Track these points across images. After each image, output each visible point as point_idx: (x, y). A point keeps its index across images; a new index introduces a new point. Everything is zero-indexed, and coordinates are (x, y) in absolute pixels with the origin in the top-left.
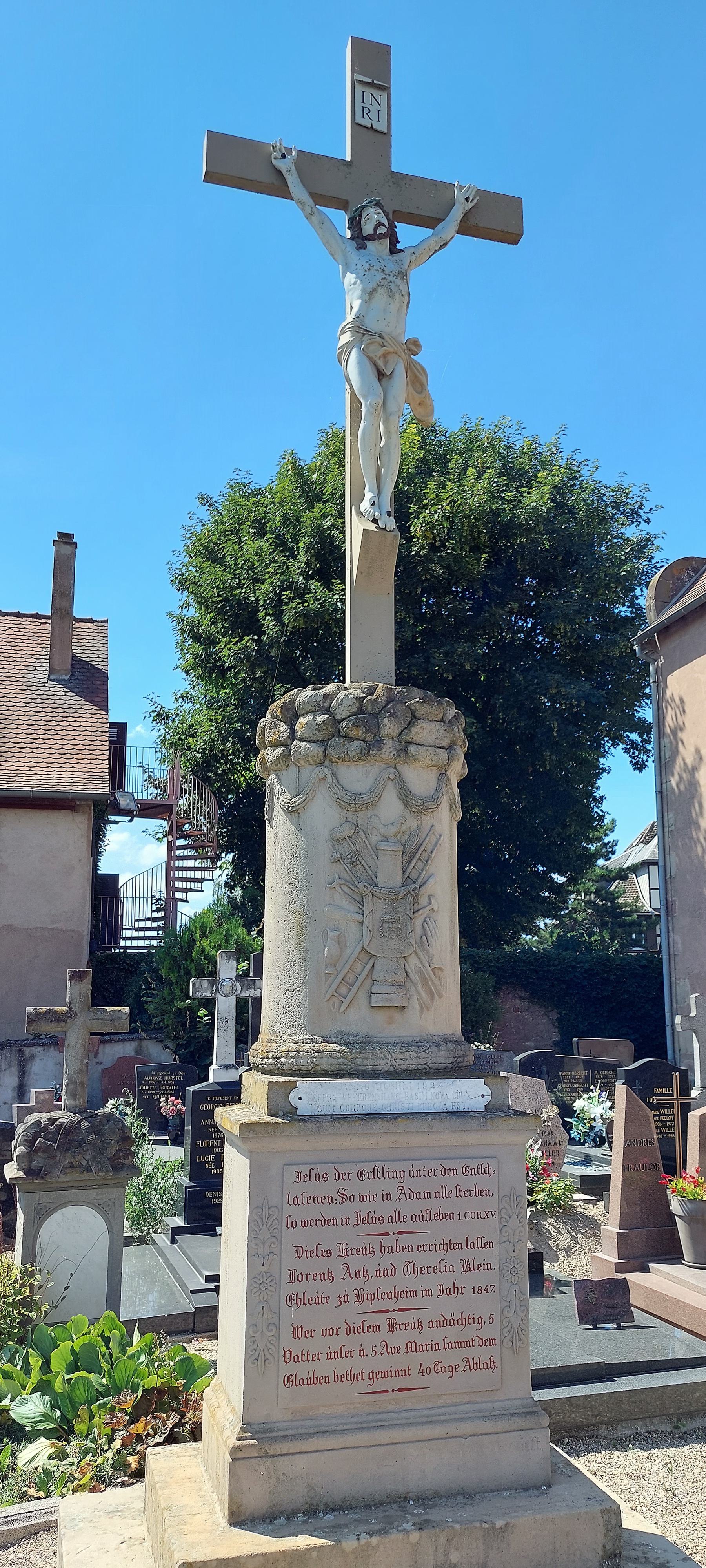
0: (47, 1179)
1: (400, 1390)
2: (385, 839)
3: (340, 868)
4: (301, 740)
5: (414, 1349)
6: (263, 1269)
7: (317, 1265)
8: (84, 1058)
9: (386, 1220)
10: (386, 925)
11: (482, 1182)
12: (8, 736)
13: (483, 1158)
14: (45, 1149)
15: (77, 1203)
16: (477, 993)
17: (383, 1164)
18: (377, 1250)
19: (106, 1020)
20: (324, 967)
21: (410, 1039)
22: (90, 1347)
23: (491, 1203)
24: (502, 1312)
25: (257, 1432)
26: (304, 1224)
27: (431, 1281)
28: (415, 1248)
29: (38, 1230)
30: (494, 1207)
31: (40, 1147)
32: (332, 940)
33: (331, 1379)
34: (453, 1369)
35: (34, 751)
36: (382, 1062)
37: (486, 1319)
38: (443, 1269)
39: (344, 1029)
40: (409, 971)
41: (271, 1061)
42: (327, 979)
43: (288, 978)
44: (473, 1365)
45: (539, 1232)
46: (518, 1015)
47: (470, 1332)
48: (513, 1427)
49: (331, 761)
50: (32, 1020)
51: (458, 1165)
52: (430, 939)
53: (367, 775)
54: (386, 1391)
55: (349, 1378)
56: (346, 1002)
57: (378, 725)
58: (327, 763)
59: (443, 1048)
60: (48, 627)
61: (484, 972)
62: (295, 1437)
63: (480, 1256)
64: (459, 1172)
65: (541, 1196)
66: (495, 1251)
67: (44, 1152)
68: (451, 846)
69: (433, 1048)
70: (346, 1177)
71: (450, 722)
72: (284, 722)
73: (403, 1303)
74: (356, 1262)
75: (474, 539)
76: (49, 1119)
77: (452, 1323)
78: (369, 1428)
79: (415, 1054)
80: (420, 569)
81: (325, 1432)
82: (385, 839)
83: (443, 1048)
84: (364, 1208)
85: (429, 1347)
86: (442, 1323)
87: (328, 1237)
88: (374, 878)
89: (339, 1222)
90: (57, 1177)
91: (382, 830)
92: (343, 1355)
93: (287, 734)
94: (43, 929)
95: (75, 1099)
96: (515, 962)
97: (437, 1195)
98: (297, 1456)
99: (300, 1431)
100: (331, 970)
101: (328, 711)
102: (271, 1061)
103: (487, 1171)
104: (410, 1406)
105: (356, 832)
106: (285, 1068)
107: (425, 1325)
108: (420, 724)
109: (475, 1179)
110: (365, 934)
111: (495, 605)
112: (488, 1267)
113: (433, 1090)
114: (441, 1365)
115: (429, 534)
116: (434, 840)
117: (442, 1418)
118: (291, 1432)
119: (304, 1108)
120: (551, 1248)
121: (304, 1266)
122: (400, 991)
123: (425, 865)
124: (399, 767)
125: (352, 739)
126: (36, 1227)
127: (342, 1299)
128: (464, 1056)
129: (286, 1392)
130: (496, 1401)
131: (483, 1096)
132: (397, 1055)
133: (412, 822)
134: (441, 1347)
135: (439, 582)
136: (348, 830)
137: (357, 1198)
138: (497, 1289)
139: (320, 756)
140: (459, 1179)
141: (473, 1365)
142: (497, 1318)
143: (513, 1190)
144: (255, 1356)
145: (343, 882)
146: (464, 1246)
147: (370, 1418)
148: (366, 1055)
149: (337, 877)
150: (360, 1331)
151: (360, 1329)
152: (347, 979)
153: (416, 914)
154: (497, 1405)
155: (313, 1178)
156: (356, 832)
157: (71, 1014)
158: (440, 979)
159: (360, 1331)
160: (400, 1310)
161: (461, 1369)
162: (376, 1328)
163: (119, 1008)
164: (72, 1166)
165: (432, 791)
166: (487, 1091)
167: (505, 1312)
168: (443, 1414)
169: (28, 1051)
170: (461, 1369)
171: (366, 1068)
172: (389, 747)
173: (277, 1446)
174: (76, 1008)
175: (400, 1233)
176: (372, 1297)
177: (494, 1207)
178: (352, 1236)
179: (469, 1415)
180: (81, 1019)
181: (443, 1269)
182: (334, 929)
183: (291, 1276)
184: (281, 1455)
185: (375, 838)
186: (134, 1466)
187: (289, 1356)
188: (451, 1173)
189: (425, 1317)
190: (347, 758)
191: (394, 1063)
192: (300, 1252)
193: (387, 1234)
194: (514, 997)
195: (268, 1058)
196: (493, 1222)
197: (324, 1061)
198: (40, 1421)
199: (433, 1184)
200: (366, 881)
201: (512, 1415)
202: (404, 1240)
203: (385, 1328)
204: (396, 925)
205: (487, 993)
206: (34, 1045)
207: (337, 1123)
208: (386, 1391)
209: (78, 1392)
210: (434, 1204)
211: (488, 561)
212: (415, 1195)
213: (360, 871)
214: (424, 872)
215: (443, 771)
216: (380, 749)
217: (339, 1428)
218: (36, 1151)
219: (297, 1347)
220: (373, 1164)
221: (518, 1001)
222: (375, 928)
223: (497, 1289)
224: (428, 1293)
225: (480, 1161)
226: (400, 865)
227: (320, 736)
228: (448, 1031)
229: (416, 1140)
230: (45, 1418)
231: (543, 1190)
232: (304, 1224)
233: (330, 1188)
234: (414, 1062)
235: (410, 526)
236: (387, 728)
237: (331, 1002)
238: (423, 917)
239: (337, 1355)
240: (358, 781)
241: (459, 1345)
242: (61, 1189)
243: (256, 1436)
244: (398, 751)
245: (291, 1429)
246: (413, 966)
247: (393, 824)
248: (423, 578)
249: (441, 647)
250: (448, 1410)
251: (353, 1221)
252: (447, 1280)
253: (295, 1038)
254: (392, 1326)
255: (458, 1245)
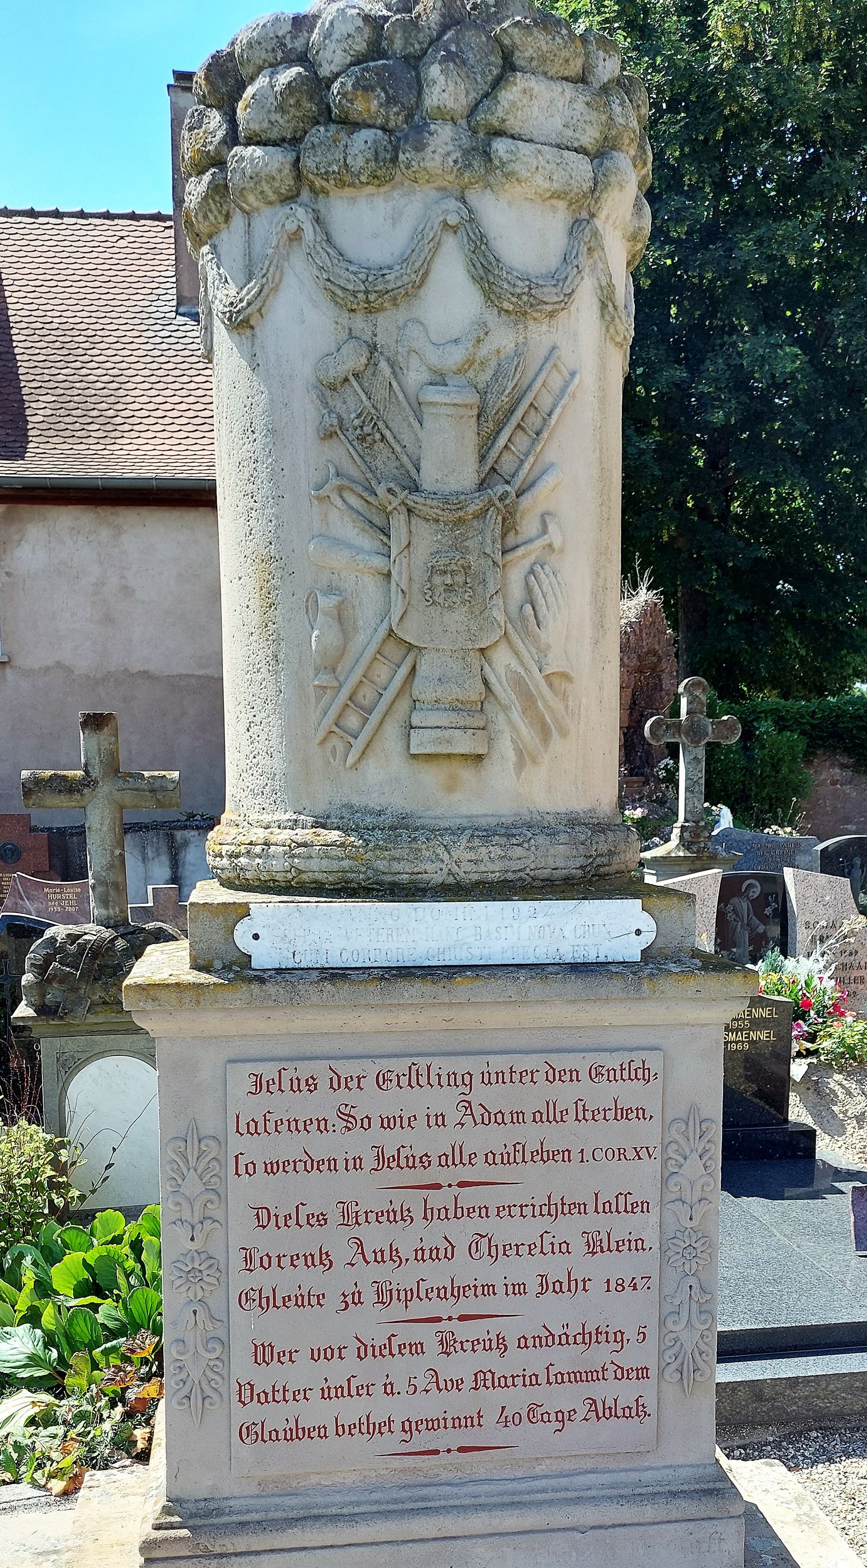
0: (68, 1020)
1: (461, 1450)
2: (439, 379)
3: (340, 453)
4: (250, 141)
5: (489, 1383)
6: (190, 1245)
7: (304, 1240)
8: (115, 848)
9: (435, 1161)
10: (437, 580)
11: (631, 1093)
12: (123, 400)
13: (631, 1050)
14: (64, 978)
15: (119, 1052)
16: (780, 760)
17: (428, 1060)
18: (418, 1213)
19: (144, 790)
20: (311, 672)
21: (493, 821)
22: (110, 1263)
23: (648, 1133)
24: (662, 1322)
25: (192, 1516)
26: (271, 1168)
27: (525, 1269)
28: (493, 1212)
29: (64, 1089)
30: (654, 1141)
31: (55, 976)
32: (326, 614)
33: (331, 1431)
34: (563, 1418)
35: (160, 421)
36: (430, 867)
37: (631, 1333)
38: (547, 1248)
39: (356, 800)
40: (492, 679)
41: (225, 862)
42: (319, 699)
43: (250, 698)
44: (601, 1411)
45: (818, 1092)
46: (837, 790)
47: (600, 1355)
48: (674, 1516)
49: (312, 189)
50: (30, 789)
51: (582, 1063)
52: (542, 610)
53: (395, 221)
54: (437, 1452)
55: (364, 1429)
56: (359, 744)
57: (419, 86)
58: (305, 195)
59: (563, 838)
60: (171, 232)
61: (792, 731)
62: (261, 1526)
63: (621, 1226)
64: (584, 1075)
65: (827, 1044)
66: (653, 1218)
67: (61, 982)
68: (603, 401)
69: (541, 839)
70: (353, 1084)
71: (605, 89)
72: (219, 108)
73: (468, 1306)
74: (375, 1236)
75: (810, 38)
76: (68, 935)
77: (565, 1340)
78: (402, 1513)
79: (499, 852)
80: (721, 95)
81: (317, 1518)
82: (439, 379)
83: (563, 838)
84: (391, 1141)
85: (519, 1381)
86: (545, 1339)
87: (319, 1192)
88: (413, 472)
89: (341, 1165)
90: (82, 1017)
91: (433, 357)
92: (354, 1392)
93: (220, 134)
94: (190, 676)
95: (107, 908)
96: (837, 716)
97: (537, 1117)
98: (264, 1557)
99: (271, 1515)
100: (325, 679)
101: (302, 58)
102: (225, 862)
103: (644, 1075)
104: (482, 1473)
105: (372, 363)
106: (249, 875)
107: (512, 1343)
108: (520, 82)
109: (616, 1089)
110: (393, 599)
111: (841, 154)
112: (637, 1245)
113: (532, 922)
114: (540, 1410)
115: (737, 31)
116: (556, 381)
117: (540, 1497)
118: (255, 1517)
119: (264, 956)
120: (834, 1115)
121: (272, 1241)
122: (469, 721)
123: (534, 442)
124: (472, 197)
125: (352, 125)
126: (61, 1084)
127: (349, 1299)
128: (611, 853)
129: (245, 1451)
130: (648, 1469)
131: (638, 932)
132: (461, 852)
133: (503, 339)
134: (542, 1379)
135: (753, 119)
136: (353, 359)
137: (376, 1123)
138: (654, 1282)
139: (287, 181)
140: (584, 1089)
141: (601, 1411)
142: (652, 1333)
143: (693, 1109)
144: (185, 1391)
145: (346, 483)
146: (591, 1208)
147: (404, 1494)
148: (397, 853)
149: (332, 471)
150: (386, 1352)
151: (386, 1350)
152: (359, 698)
153: (509, 557)
154: (647, 1476)
155: (286, 1085)
156: (372, 363)
157: (88, 782)
158: (564, 697)
159: (386, 1352)
160: (462, 1318)
161: (580, 1416)
162: (417, 1348)
163: (163, 773)
164: (105, 1003)
165: (554, 261)
166: (647, 923)
167: (669, 1324)
168: (544, 1491)
169: (179, 835)
170: (580, 1416)
171: (397, 878)
172: (443, 140)
173: (226, 1541)
174: (95, 773)
175: (462, 1184)
176: (408, 1296)
177: (654, 1141)
178: (368, 1190)
179: (593, 1493)
180: (105, 788)
181: (547, 1248)
182: (330, 590)
183: (249, 1259)
184: (236, 1555)
185: (415, 376)
186: (141, 1445)
187: (248, 1393)
188: (567, 1078)
189: (511, 1330)
190: (346, 178)
191: (455, 869)
192: (264, 1217)
193: (438, 1186)
194: (832, 766)
195: (221, 856)
196: (651, 1168)
197: (314, 864)
198: (25, 1366)
199: (532, 1098)
200: (395, 479)
201: (674, 1494)
202: (470, 1197)
203: (432, 1346)
204: (460, 579)
205: (794, 759)
206: (185, 828)
207: (328, 986)
208: (437, 1452)
209: (78, 1329)
210: (531, 1135)
211: (833, 75)
212: (492, 1118)
213: (383, 460)
214: (531, 459)
215: (584, 215)
216: (420, 147)
217: (345, 1511)
218: (49, 981)
219: (263, 1378)
220: (408, 1061)
221: (837, 770)
222: (416, 587)
223: (654, 1282)
224: (519, 1289)
225: (626, 1057)
226: (471, 440)
227: (284, 125)
228: (578, 804)
229: (494, 1016)
230: (33, 1360)
231: (830, 1035)
232: (271, 1168)
233: (322, 1103)
234: (497, 866)
235: (707, 19)
236: (437, 89)
237: (329, 745)
238: (526, 564)
239: (342, 1392)
240: (376, 236)
241: (576, 1377)
242: (92, 1033)
243: (191, 1523)
244: (466, 153)
245: (257, 1511)
246: (502, 671)
247: (456, 341)
248: (727, 112)
249: (751, 230)
250: (553, 1482)
251: (370, 1161)
252: (555, 1267)
253: (266, 818)
254: (447, 1346)
255: (581, 1208)
